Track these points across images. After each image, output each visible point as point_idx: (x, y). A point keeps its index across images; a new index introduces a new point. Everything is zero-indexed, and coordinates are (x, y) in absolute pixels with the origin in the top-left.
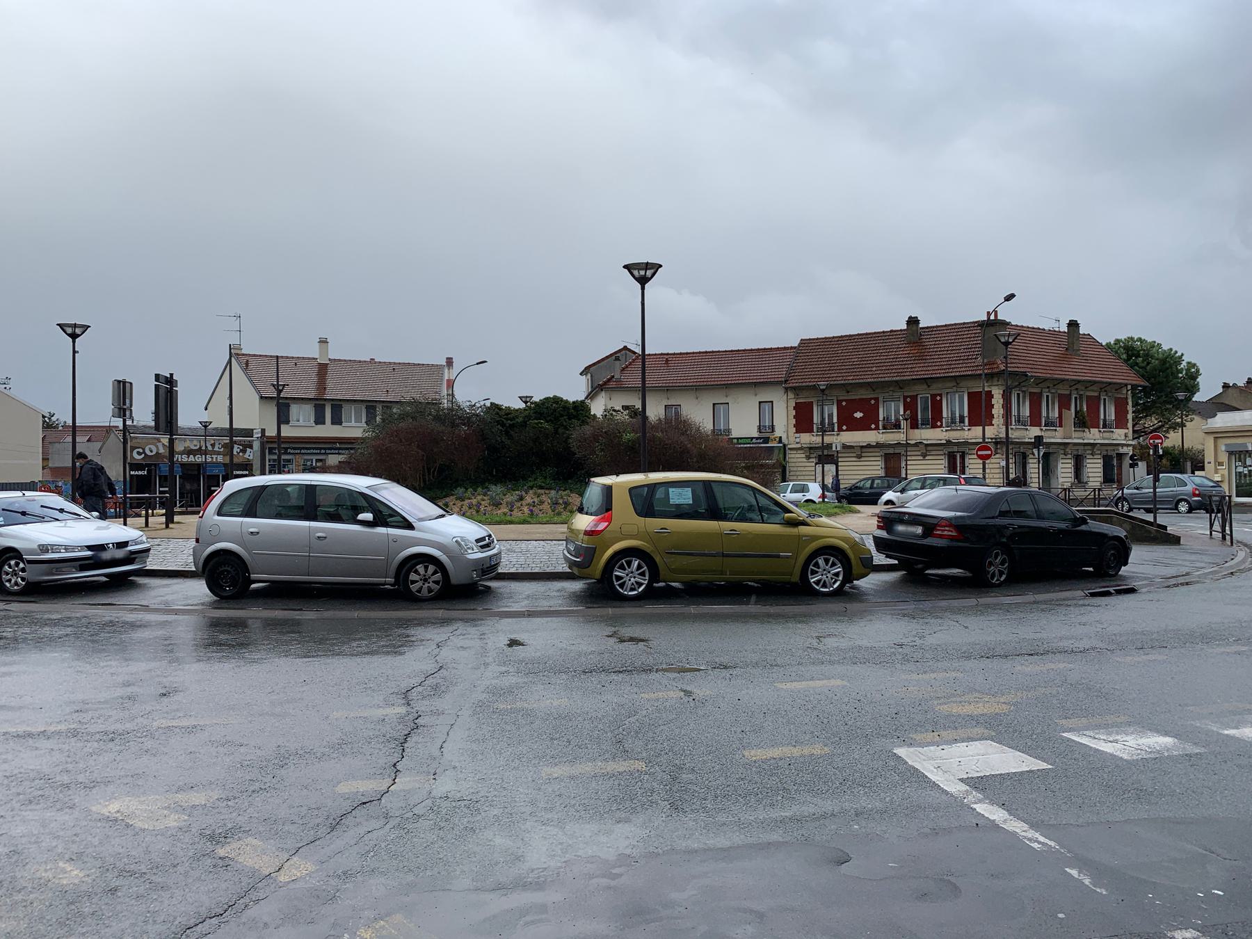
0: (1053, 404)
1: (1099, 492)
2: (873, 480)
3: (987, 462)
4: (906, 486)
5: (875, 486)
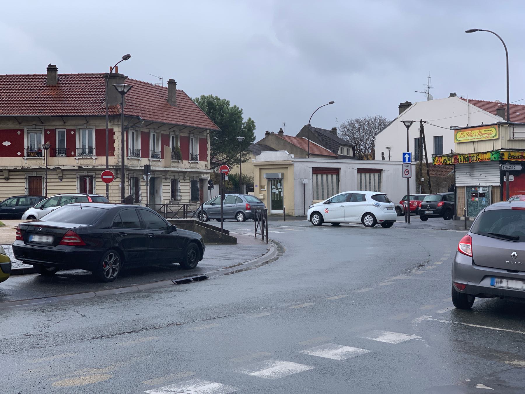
0: (158, 140)
1: (187, 207)
2: (18, 198)
3: (110, 184)
4: (45, 203)
5: (20, 203)
